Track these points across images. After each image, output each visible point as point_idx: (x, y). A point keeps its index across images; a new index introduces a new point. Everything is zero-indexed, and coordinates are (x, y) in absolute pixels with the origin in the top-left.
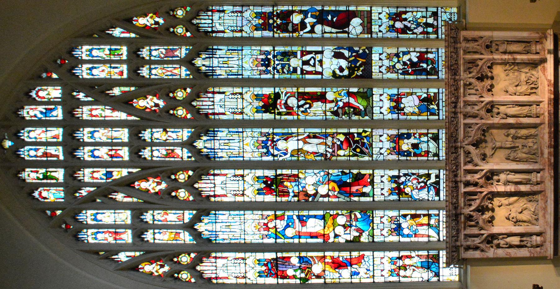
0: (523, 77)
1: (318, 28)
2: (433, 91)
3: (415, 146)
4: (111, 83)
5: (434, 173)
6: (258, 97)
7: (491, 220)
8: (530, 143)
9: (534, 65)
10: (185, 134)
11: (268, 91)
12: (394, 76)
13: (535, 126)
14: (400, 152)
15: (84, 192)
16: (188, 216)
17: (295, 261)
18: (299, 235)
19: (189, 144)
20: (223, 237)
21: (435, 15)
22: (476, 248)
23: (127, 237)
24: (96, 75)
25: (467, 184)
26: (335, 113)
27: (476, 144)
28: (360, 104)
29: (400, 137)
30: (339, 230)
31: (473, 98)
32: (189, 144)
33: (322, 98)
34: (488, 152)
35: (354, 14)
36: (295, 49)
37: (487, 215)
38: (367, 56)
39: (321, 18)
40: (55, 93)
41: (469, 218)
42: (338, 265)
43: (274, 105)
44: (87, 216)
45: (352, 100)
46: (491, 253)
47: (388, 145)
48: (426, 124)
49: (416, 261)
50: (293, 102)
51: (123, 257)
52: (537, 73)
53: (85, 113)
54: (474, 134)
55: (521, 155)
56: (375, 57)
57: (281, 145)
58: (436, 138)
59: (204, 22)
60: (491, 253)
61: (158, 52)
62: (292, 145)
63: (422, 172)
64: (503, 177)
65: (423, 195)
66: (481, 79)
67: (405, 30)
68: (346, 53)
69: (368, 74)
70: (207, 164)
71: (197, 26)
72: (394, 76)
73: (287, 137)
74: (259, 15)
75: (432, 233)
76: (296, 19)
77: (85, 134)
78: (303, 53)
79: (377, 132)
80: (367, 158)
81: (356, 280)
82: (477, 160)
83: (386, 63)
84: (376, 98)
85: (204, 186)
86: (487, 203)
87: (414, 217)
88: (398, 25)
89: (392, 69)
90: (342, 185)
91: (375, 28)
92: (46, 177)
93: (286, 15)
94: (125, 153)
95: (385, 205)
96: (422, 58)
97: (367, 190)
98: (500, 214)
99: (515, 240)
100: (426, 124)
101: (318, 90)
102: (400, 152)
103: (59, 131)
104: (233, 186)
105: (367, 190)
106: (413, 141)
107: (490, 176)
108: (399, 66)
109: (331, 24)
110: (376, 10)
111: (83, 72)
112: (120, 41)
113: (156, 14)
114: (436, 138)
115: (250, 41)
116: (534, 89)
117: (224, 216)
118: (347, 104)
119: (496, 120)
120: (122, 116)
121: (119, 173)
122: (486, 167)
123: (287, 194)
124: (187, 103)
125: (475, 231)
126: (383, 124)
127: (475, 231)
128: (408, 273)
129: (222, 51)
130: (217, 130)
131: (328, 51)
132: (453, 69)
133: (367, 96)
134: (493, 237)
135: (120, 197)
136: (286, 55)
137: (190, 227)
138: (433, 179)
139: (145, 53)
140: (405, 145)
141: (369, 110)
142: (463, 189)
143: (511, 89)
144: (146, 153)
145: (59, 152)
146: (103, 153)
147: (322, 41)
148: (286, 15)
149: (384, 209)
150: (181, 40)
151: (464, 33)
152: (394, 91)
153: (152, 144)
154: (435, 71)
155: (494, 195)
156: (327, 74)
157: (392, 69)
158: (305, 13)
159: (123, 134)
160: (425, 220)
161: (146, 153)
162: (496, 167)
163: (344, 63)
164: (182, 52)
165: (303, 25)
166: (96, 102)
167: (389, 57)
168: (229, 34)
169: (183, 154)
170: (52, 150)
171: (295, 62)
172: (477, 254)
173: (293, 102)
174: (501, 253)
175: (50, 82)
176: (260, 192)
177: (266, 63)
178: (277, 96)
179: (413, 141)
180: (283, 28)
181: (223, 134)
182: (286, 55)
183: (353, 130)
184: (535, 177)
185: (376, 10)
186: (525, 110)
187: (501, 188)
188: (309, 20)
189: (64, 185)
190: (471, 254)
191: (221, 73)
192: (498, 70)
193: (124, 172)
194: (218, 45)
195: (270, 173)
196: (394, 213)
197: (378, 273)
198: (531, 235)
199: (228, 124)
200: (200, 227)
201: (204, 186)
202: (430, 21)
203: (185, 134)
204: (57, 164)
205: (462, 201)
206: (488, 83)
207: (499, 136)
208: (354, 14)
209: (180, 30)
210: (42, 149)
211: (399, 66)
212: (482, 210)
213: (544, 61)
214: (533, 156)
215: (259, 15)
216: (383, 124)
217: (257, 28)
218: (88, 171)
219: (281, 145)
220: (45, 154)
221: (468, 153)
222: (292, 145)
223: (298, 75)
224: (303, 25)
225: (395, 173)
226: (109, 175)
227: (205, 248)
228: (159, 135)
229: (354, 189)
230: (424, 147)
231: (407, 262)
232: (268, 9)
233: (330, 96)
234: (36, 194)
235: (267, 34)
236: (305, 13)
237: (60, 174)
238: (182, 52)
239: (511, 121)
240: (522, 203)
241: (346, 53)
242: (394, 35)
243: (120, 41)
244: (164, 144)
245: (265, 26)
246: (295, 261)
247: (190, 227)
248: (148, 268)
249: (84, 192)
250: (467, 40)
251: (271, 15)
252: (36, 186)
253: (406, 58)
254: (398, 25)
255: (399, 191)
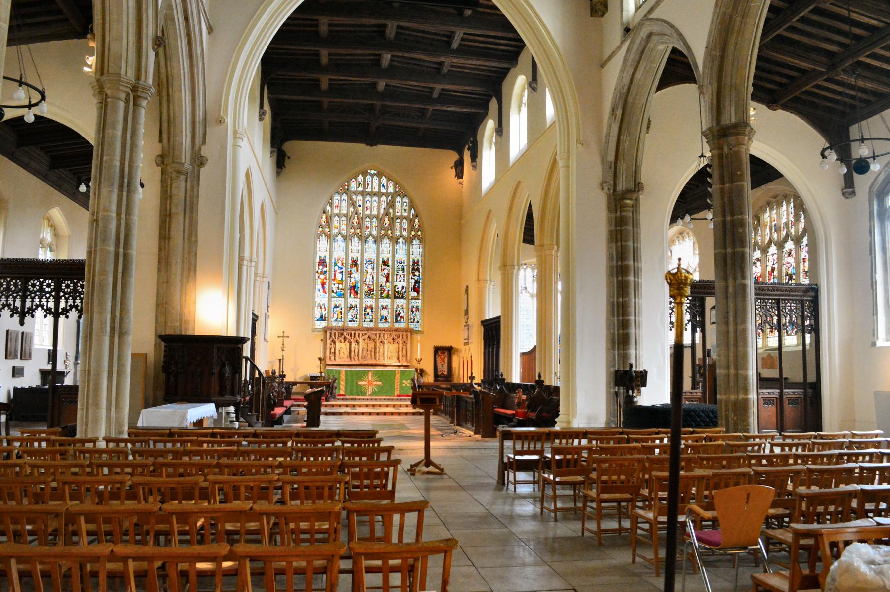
0: (394, 354)
1: (413, 281)
2: (389, 320)
3: (368, 314)
4: (394, 209)
5: (358, 320)
6: (388, 259)
7: (341, 342)
8: (369, 356)
9: (398, 358)
10: (375, 233)
11: (390, 263)
12: (395, 307)
13: (375, 358)
14: (366, 308)
15: (354, 197)
17: (325, 269)
18: (335, 271)
19: (371, 235)
21: (418, 322)
22: (330, 336)
23: (336, 211)
25: (355, 334)
26: (381, 286)
27: (369, 337)
28: (384, 295)
29: (372, 309)
30: (337, 285)
31: (386, 337)
32: (371, 235)
33: (387, 281)
34: (366, 341)
35: (418, 293)
36: (406, 272)
37: (343, 340)
38: (402, 297)
39: (417, 282)
40: (391, 190)
41: (342, 334)
42: (323, 284)
43: (385, 264)
45: (386, 292)
46: (329, 342)
47: (369, 305)
48: (377, 318)
49: (324, 313)
50: (386, 271)
51: (329, 208)
52: (395, 359)
54: (373, 337)
55: (365, 352)
56: (402, 300)
57: (370, 266)
58: (371, 321)
59: (416, 242)
60: (329, 342)
61: (406, 225)
62: (370, 270)
63: (358, 316)
64: (357, 346)
65: (349, 316)
66: (393, 339)
67: (412, 311)
68: (404, 290)
69: (396, 297)
70: (394, 241)
71: (322, 235)
72: (395, 307)
73: (373, 268)
74: (418, 260)
75: (334, 319)
76: (417, 273)
78: (404, 275)
79: (374, 300)
80: (364, 296)
81: (317, 290)
82: (364, 337)
83: (400, 305)
84: (387, 300)
86: (347, 341)
87: (341, 313)
88: (414, 309)
89: (398, 306)
90: (354, 287)
91: (413, 301)
92: (360, 184)
93: (418, 270)
94: (368, 212)
95: (346, 302)
96: (402, 317)
97: (352, 296)
98: (343, 345)
99: (333, 350)
100: (377, 318)
101: (390, 280)
102: (366, 308)
103: (376, 190)
104: (355, 250)
105: (352, 296)
106: (370, 313)
107: (357, 342)
108: (399, 309)
109: (415, 286)
110: (420, 301)
111: (398, 199)
112: (409, 212)
113: (389, 224)
114: (371, 321)
115: (409, 257)
116: (389, 358)
118: (384, 290)
119: (378, 344)
120: (382, 211)
121: (360, 210)
122: (361, 340)
123: (351, 267)
125: (337, 336)
126: (377, 302)
127: (337, 336)
128: (319, 309)
129: (375, 246)
131: (405, 284)
132: (397, 330)
133: (388, 297)
134: (334, 342)
136: (403, 269)
138: (355, 320)
139: (405, 221)
140: (369, 310)
141: (382, 297)
142: (353, 332)
143: (389, 350)
145: (369, 190)
147: (409, 282)
148: (418, 270)
149: (345, 302)
150: (379, 232)
151: (409, 334)
152: (389, 307)
153: (371, 222)
154: (397, 321)
155: (350, 343)
156: (395, 284)
157: (398, 306)
158: (419, 277)
159: (375, 212)
160: (340, 316)
162: (361, 344)
163: (400, 289)
164: (405, 234)
165: (414, 276)
166: (388, 204)
167: (402, 305)
168: (411, 250)
170: (370, 187)
171: (401, 272)
172: (328, 336)
173: (386, 271)
174: (328, 345)
175: (395, 188)
176: (352, 258)
177: (401, 262)
178: (388, 266)
179: (370, 313)
180: (413, 269)
181: (343, 245)
182: (403, 269)
183: (375, 292)
184: (356, 358)
185: (420, 301)
186: (381, 355)
187: (353, 345)
188: (416, 278)
189: (357, 191)
190: (328, 335)
191: (397, 247)
192: (396, 345)
193: (361, 211)
195: (359, 262)
196: (343, 306)
197: (319, 299)
198: (335, 356)
202: (416, 321)
203: (375, 233)
204: (364, 188)
205: (349, 332)
206: (392, 341)
207: (372, 345)
208: (418, 293)
209: (413, 233)
210: (370, 183)
211: (399, 309)
212: (345, 339)
213: (399, 362)
214: (365, 357)
215: (418, 260)
216: (377, 302)
217: (414, 260)
218: (361, 198)
219: (370, 266)
220: (368, 184)
221: (366, 334)
222: (370, 270)
223: (396, 273)
224: (414, 276)
225: (358, 306)
226: (360, 206)
227: (332, 238)
228: (375, 224)
229: (352, 291)
230: (368, 316)
231: (323, 310)
232: (420, 264)
233: (388, 284)
234: (353, 180)
235: (411, 263)
236: (419, 277)
238: (405, 234)
239: (378, 350)
240: (347, 353)
241: (404, 290)
242: (411, 307)
243: (409, 212)
244: (371, 226)
245: (414, 263)
246: (325, 269)
248: (324, 217)
249: (354, 197)
250: (407, 335)
251: (418, 265)
252: (356, 180)
253: (402, 311)
254: (414, 309)
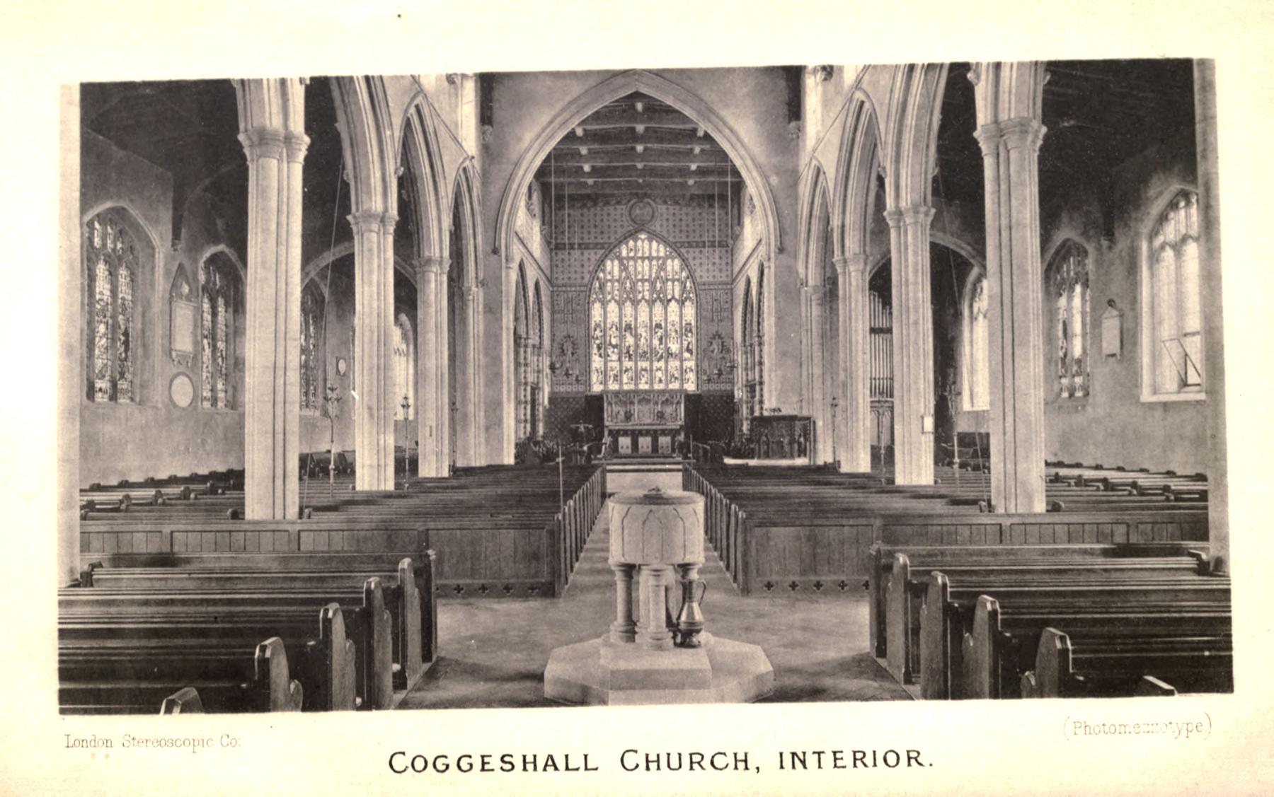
16: (677, 297)
20: (669, 309)
24: (1153, 275)
33: (661, 343)
44: (616, 262)
53: (654, 262)
62: (644, 334)
77: (647, 262)
85: (658, 304)
117: (648, 310)
120: (653, 275)
124: (659, 297)
130: (1088, 298)
135: (624, 274)
137: (673, 297)
144: (640, 284)
145: (640, 254)
146: (640, 269)
161: (640, 284)
169: (640, 297)
194: (1092, 298)
199: (651, 311)
200: (673, 301)
201: (628, 304)
204: (636, 254)
237: (632, 254)
247: (673, 297)
255: (626, 371)
